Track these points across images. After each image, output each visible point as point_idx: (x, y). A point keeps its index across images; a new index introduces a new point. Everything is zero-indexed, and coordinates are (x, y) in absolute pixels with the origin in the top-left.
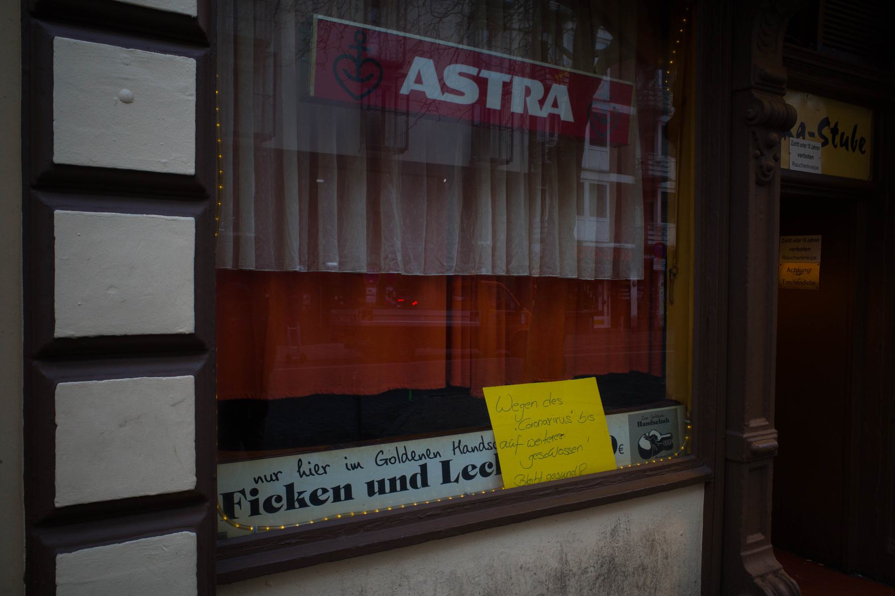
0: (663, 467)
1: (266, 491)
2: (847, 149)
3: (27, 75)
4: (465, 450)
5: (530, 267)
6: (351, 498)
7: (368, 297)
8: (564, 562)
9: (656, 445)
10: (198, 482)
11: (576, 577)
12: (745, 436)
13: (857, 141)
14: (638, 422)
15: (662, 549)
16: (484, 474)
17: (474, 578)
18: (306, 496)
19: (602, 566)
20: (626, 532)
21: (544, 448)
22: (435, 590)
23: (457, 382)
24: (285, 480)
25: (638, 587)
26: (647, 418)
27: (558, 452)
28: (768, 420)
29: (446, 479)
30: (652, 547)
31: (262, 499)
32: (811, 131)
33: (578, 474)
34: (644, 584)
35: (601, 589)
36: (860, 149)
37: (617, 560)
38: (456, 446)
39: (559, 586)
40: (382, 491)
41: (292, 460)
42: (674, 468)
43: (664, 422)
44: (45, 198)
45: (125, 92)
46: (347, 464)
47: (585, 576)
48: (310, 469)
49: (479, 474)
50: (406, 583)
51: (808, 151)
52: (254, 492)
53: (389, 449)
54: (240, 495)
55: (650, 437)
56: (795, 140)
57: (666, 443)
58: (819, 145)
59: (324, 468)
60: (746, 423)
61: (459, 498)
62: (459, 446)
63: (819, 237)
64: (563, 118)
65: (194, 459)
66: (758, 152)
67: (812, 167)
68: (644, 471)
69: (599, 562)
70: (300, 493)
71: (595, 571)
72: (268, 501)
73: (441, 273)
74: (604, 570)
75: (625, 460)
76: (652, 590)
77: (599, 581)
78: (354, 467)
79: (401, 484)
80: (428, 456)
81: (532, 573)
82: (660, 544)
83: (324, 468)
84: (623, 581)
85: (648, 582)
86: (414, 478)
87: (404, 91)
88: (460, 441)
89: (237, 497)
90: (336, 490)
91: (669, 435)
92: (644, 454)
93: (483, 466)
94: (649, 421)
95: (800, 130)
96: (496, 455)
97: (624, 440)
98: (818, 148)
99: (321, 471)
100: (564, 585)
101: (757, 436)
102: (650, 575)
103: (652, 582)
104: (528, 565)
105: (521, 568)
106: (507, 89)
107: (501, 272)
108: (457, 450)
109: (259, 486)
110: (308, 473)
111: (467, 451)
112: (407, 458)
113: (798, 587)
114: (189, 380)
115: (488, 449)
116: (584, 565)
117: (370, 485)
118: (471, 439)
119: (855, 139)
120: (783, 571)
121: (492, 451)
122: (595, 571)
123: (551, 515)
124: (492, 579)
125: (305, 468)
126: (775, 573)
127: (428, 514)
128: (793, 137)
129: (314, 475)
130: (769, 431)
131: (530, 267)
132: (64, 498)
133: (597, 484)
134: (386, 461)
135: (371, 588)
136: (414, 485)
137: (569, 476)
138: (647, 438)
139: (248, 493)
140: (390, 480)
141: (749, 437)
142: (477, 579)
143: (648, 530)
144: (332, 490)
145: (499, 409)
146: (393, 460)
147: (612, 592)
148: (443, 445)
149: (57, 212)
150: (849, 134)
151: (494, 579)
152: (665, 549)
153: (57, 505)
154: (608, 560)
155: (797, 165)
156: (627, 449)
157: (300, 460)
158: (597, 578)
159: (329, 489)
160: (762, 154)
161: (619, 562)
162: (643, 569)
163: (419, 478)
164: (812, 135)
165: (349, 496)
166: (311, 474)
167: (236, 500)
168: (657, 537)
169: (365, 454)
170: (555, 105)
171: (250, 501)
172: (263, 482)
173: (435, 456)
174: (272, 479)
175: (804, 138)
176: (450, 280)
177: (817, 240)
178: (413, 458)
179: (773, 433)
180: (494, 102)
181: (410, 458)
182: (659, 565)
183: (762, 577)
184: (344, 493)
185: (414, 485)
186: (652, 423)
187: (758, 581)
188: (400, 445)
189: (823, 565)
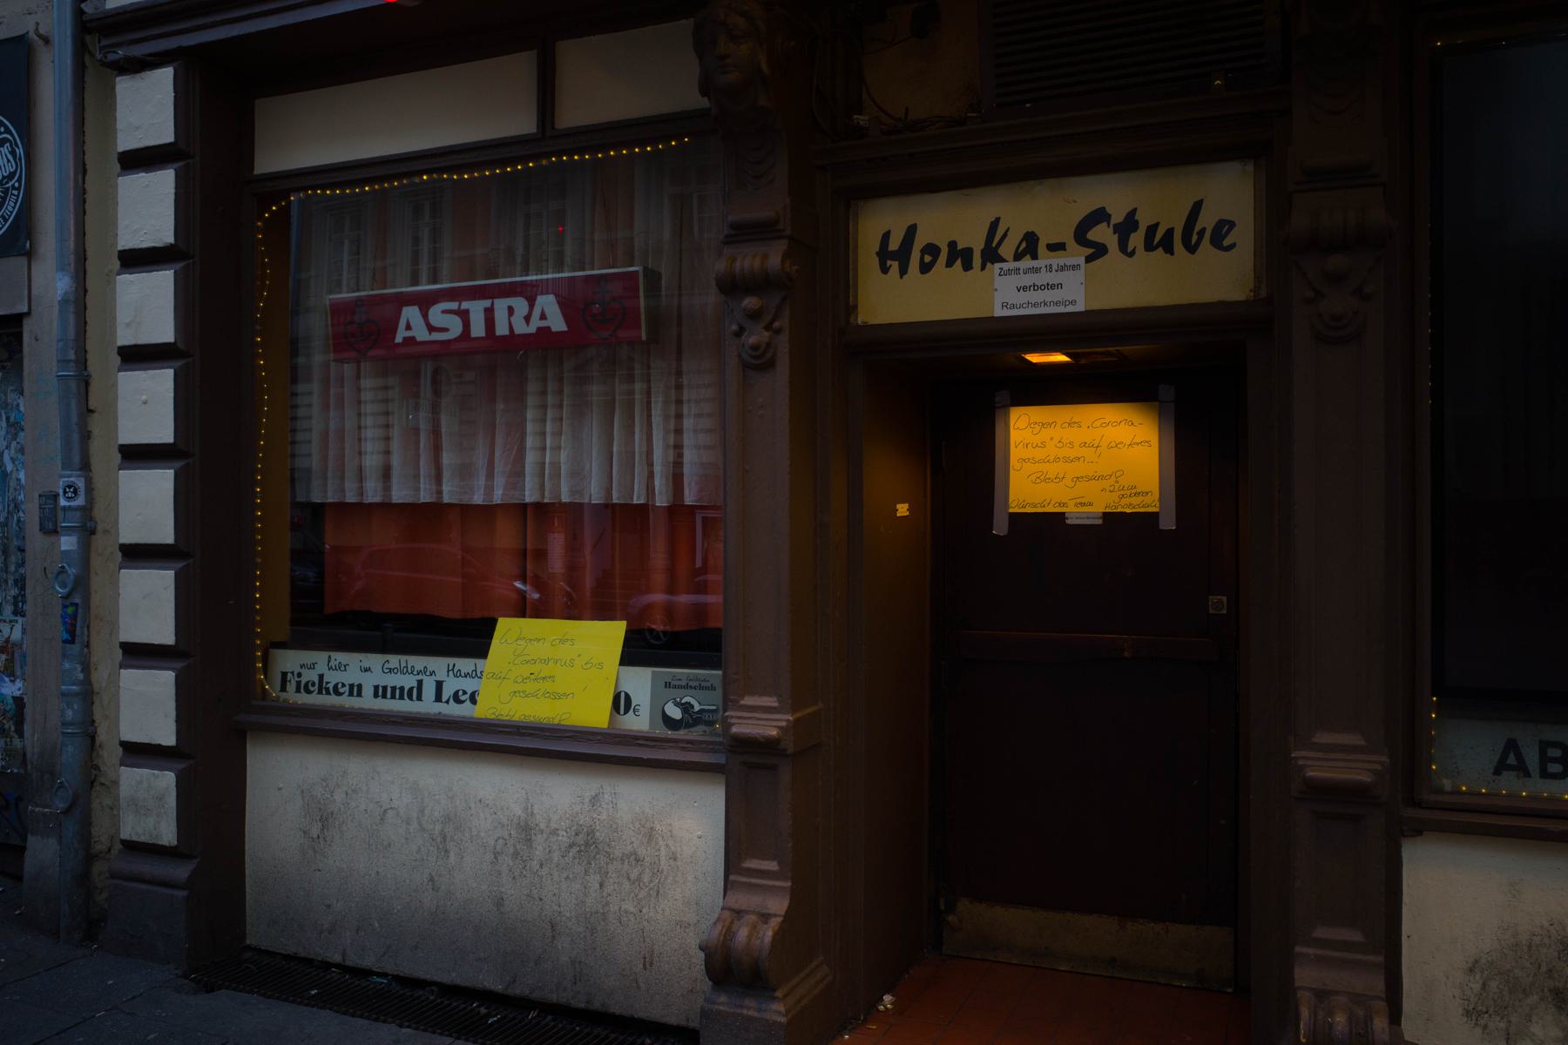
4: (458, 675)
6: (361, 696)
8: (530, 813)
9: (691, 716)
11: (545, 835)
14: (666, 683)
15: (667, 846)
17: (435, 795)
18: (331, 686)
19: (577, 834)
21: (530, 687)
22: (401, 793)
25: (629, 879)
26: (680, 680)
29: (438, 698)
33: (556, 722)
34: (639, 879)
35: (577, 861)
37: (598, 834)
42: (682, 745)
43: (706, 688)
45: (144, 397)
53: (394, 660)
55: (683, 704)
56: (1012, 265)
57: (706, 717)
58: (1081, 261)
59: (345, 666)
64: (555, 329)
67: (1056, 304)
70: (327, 683)
72: (306, 685)
74: (580, 839)
76: (652, 892)
79: (399, 693)
82: (663, 837)
85: (646, 879)
86: (411, 689)
87: (399, 339)
88: (454, 665)
89: (289, 675)
91: (714, 708)
92: (668, 721)
94: (683, 683)
95: (1024, 245)
98: (1075, 267)
99: (343, 668)
102: (647, 870)
103: (651, 881)
104: (487, 802)
106: (489, 313)
109: (303, 671)
116: (553, 826)
118: (465, 664)
119: (1197, 228)
123: (464, 749)
128: (1004, 260)
133: (567, 737)
134: (391, 670)
137: (545, 721)
138: (677, 704)
140: (392, 688)
141: (732, 717)
142: (437, 797)
146: (395, 671)
148: (439, 665)
152: (673, 848)
156: (645, 712)
157: (330, 657)
158: (571, 846)
161: (601, 839)
163: (415, 691)
165: (359, 694)
166: (336, 669)
168: (658, 827)
169: (375, 660)
173: (431, 675)
180: (478, 330)
181: (410, 671)
182: (662, 863)
184: (356, 690)
186: (687, 687)
188: (403, 658)
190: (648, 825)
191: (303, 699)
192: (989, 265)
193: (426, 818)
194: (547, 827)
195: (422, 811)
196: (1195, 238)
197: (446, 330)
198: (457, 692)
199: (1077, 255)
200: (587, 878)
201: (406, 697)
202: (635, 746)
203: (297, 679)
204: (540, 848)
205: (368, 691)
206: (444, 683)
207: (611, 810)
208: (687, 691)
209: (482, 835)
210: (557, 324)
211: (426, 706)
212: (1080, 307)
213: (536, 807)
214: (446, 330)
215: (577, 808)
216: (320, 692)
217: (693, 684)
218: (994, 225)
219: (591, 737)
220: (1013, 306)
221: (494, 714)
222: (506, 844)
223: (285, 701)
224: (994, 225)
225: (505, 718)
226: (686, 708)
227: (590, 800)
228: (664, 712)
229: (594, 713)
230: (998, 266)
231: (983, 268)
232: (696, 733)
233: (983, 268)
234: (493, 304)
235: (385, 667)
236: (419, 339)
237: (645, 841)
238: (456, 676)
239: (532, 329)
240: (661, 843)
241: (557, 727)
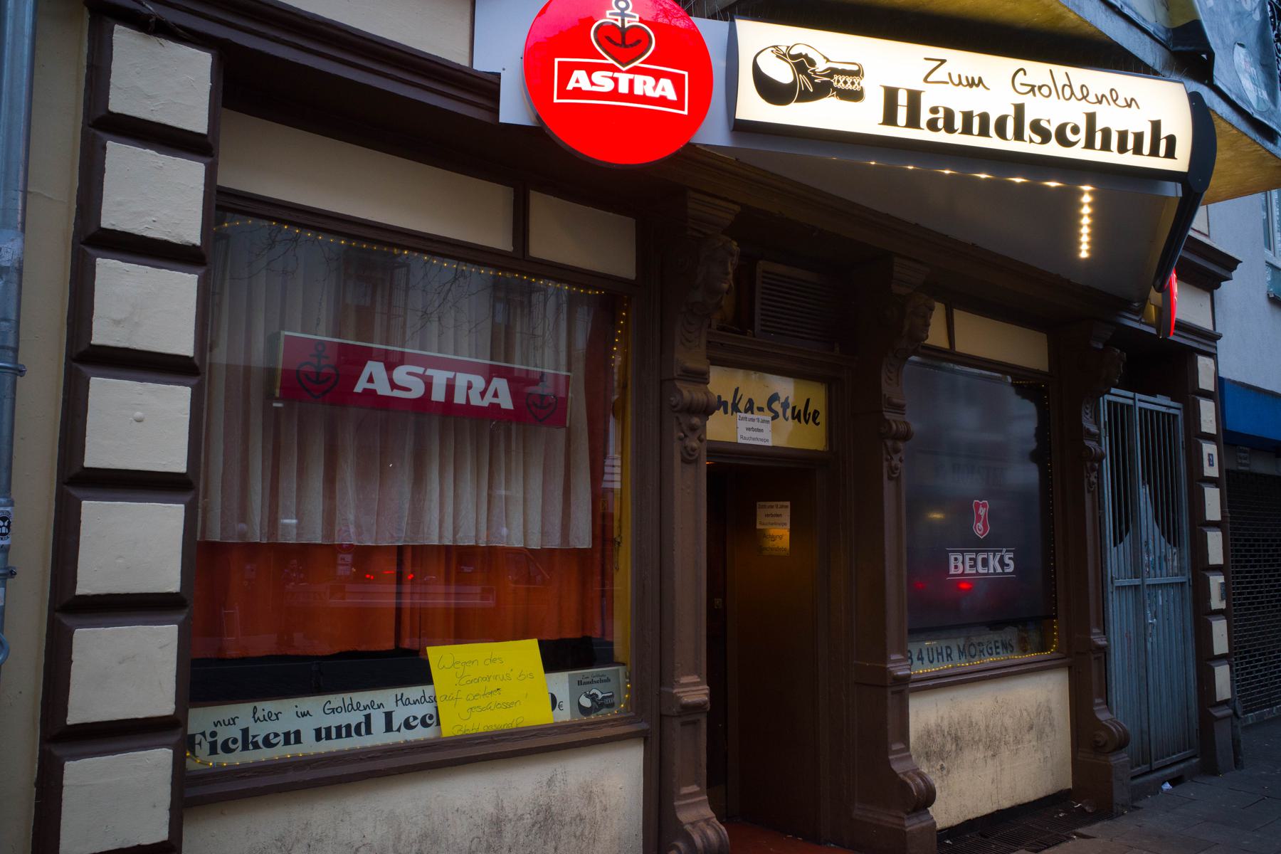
0: (602, 722)
1: (224, 734)
2: (799, 421)
3: (66, 402)
5: (477, 537)
7: (341, 568)
10: (176, 709)
11: (513, 823)
12: (675, 691)
13: (810, 413)
15: (601, 802)
16: (424, 724)
17: (412, 818)
18: (260, 740)
19: (538, 814)
20: (562, 782)
21: (483, 702)
22: (375, 827)
23: (407, 643)
24: (242, 724)
25: (575, 837)
27: (496, 706)
28: (699, 676)
29: (389, 728)
30: (590, 798)
31: (220, 740)
32: (760, 406)
33: (514, 726)
34: (582, 834)
35: (538, 836)
36: (814, 420)
37: (553, 808)
38: (398, 699)
39: (495, 830)
40: (328, 737)
41: (248, 707)
43: (605, 681)
44: (75, 492)
45: (138, 414)
46: (297, 712)
47: (521, 822)
48: (264, 716)
49: (419, 725)
50: (348, 819)
51: (756, 425)
52: (214, 734)
53: (336, 700)
54: (201, 737)
56: (743, 415)
57: (607, 701)
58: (770, 419)
59: (276, 715)
60: (676, 680)
61: (399, 743)
62: (401, 699)
63: (788, 503)
65: (174, 690)
66: (682, 435)
67: (762, 440)
68: (580, 725)
69: (535, 810)
71: (531, 818)
72: (225, 743)
73: (391, 543)
75: (565, 715)
77: (536, 828)
78: (304, 715)
79: (348, 731)
80: (372, 707)
81: (468, 816)
83: (276, 715)
84: (560, 830)
86: (358, 726)
87: (358, 389)
88: (402, 694)
90: (287, 735)
91: (611, 694)
92: (583, 710)
93: (424, 718)
95: (748, 405)
96: (437, 708)
97: (564, 696)
98: (768, 422)
99: (274, 717)
100: (499, 829)
101: (688, 691)
102: (588, 825)
103: (590, 833)
104: (464, 809)
105: (457, 811)
107: (448, 541)
108: (400, 702)
109: (218, 729)
110: (262, 719)
111: (409, 703)
112: (353, 708)
113: (726, 832)
114: (174, 628)
115: (429, 702)
116: (519, 812)
117: (318, 731)
118: (413, 692)
119: (808, 412)
120: (715, 819)
121: (434, 704)
122: (531, 818)
124: (429, 820)
125: (260, 714)
126: (707, 821)
127: (370, 756)
128: (740, 412)
129: (266, 721)
130: (701, 687)
131: (477, 536)
132: (75, 717)
133: (532, 736)
134: (333, 710)
135: (315, 822)
136: (358, 733)
137: (505, 728)
138: (587, 696)
139: (208, 735)
143: (585, 782)
144: (283, 735)
145: (441, 666)
146: (339, 710)
147: (549, 840)
148: (386, 697)
149: (84, 502)
150: (801, 407)
151: (431, 820)
152: (604, 802)
153: (68, 723)
154: (544, 809)
155: (745, 438)
156: (566, 706)
157: (255, 708)
158: (533, 826)
159: (280, 733)
160: (686, 436)
161: (556, 812)
162: (581, 820)
164: (761, 409)
165: (298, 741)
167: (197, 741)
168: (595, 789)
169: (313, 704)
170: (496, 395)
171: (210, 742)
172: (221, 725)
173: (379, 708)
174: (229, 724)
175: (752, 413)
176: (400, 550)
177: (786, 507)
178: (358, 709)
179: (705, 689)
181: (355, 708)
183: (693, 824)
185: (358, 733)
187: (688, 828)
189: (791, 836)
190: (588, 791)
191: (225, 760)
192: (734, 413)
193: (403, 842)
194: (515, 815)
195: (399, 838)
196: (807, 416)
197: (408, 390)
198: (408, 719)
199: (767, 416)
200: (546, 847)
201: (353, 734)
202: (580, 731)
203: (210, 739)
204: (509, 835)
205: (308, 736)
206: (393, 714)
207: (563, 785)
208: (595, 685)
209: (458, 841)
210: (506, 403)
211: (379, 738)
212: (770, 444)
213: (505, 801)
214: (408, 390)
215: (538, 792)
216: (245, 748)
217: (595, 679)
218: (737, 390)
219: (550, 732)
220: (745, 438)
221: (460, 730)
222: (480, 841)
223: (220, 766)
224: (737, 390)
225: (471, 732)
226: (593, 697)
227: (547, 783)
228: (579, 703)
229: (541, 715)
230: (739, 414)
231: (732, 414)
232: (605, 714)
233: (732, 414)
234: (455, 376)
235: (326, 709)
236: (380, 392)
237: (587, 802)
238: (405, 705)
239: (485, 403)
240: (597, 801)
241: (554, 725)
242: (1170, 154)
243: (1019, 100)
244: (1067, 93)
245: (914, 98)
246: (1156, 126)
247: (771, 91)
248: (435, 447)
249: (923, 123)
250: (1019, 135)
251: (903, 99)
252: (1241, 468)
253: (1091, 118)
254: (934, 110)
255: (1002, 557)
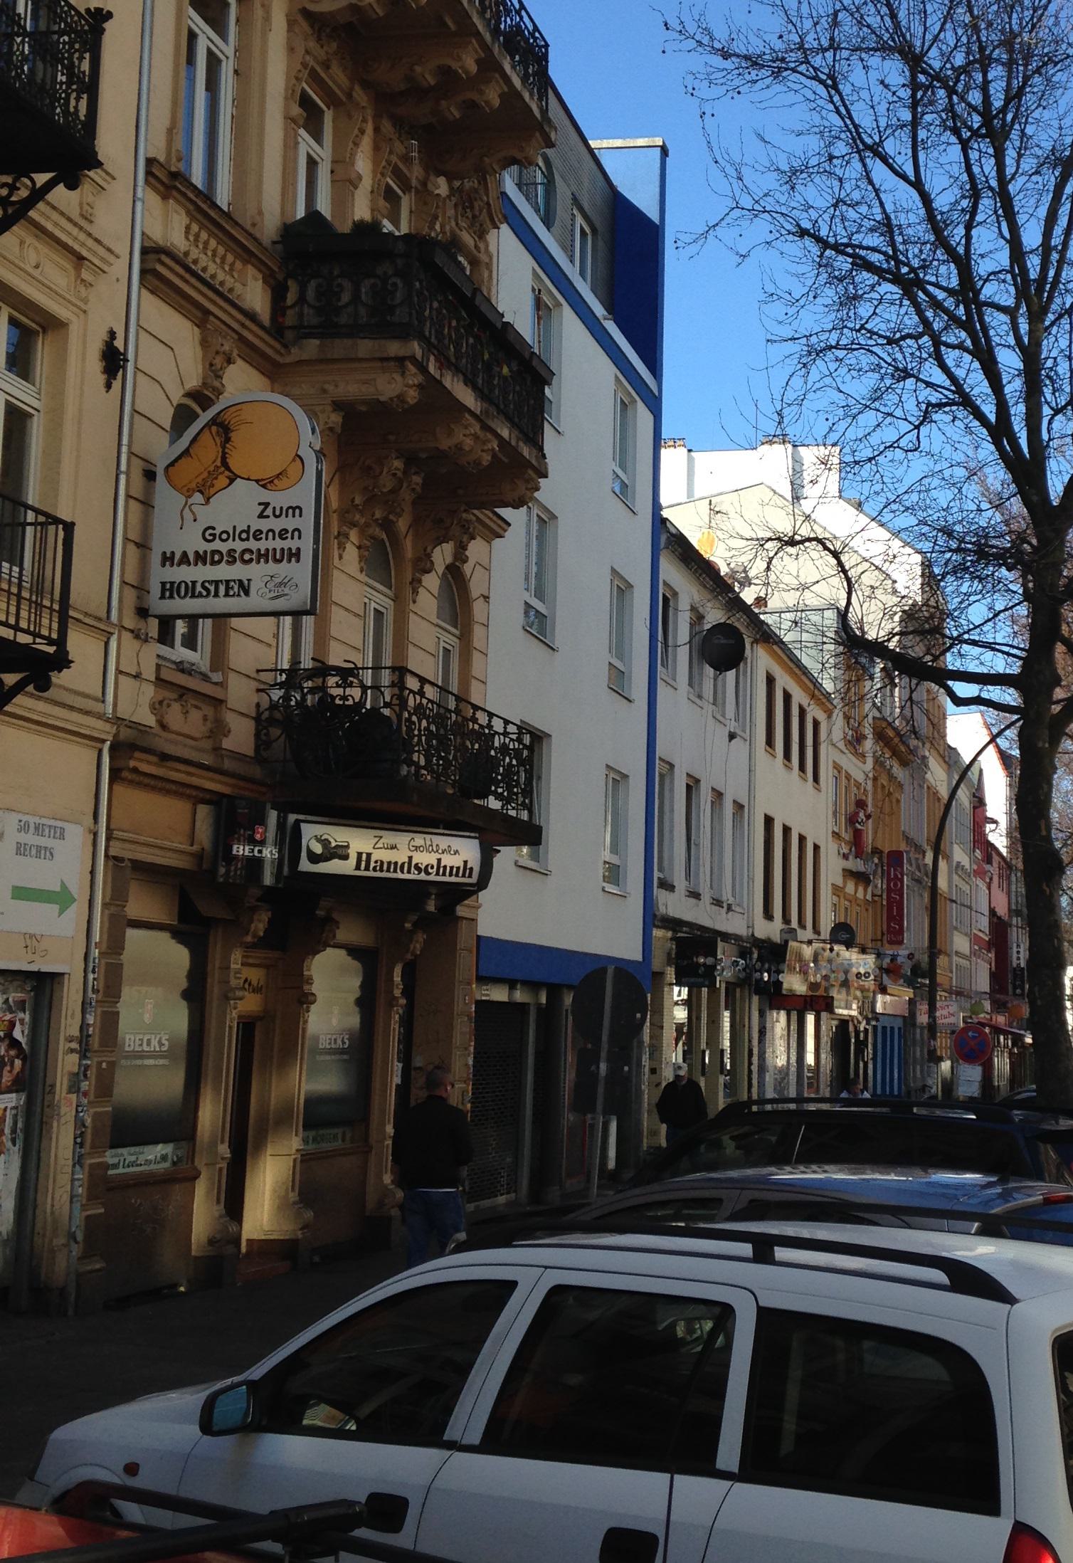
119: (19, 1143)
242: (470, 876)
243: (410, 854)
244: (429, 849)
245: (369, 855)
246: (466, 862)
247: (314, 858)
248: (274, 1073)
249: (371, 868)
250: (409, 872)
251: (364, 857)
252: (484, 998)
253: (439, 860)
254: (376, 862)
255: (160, 1038)
